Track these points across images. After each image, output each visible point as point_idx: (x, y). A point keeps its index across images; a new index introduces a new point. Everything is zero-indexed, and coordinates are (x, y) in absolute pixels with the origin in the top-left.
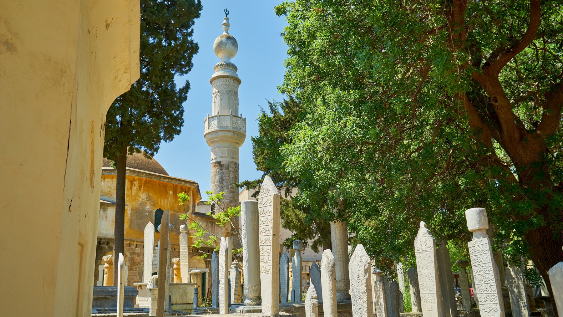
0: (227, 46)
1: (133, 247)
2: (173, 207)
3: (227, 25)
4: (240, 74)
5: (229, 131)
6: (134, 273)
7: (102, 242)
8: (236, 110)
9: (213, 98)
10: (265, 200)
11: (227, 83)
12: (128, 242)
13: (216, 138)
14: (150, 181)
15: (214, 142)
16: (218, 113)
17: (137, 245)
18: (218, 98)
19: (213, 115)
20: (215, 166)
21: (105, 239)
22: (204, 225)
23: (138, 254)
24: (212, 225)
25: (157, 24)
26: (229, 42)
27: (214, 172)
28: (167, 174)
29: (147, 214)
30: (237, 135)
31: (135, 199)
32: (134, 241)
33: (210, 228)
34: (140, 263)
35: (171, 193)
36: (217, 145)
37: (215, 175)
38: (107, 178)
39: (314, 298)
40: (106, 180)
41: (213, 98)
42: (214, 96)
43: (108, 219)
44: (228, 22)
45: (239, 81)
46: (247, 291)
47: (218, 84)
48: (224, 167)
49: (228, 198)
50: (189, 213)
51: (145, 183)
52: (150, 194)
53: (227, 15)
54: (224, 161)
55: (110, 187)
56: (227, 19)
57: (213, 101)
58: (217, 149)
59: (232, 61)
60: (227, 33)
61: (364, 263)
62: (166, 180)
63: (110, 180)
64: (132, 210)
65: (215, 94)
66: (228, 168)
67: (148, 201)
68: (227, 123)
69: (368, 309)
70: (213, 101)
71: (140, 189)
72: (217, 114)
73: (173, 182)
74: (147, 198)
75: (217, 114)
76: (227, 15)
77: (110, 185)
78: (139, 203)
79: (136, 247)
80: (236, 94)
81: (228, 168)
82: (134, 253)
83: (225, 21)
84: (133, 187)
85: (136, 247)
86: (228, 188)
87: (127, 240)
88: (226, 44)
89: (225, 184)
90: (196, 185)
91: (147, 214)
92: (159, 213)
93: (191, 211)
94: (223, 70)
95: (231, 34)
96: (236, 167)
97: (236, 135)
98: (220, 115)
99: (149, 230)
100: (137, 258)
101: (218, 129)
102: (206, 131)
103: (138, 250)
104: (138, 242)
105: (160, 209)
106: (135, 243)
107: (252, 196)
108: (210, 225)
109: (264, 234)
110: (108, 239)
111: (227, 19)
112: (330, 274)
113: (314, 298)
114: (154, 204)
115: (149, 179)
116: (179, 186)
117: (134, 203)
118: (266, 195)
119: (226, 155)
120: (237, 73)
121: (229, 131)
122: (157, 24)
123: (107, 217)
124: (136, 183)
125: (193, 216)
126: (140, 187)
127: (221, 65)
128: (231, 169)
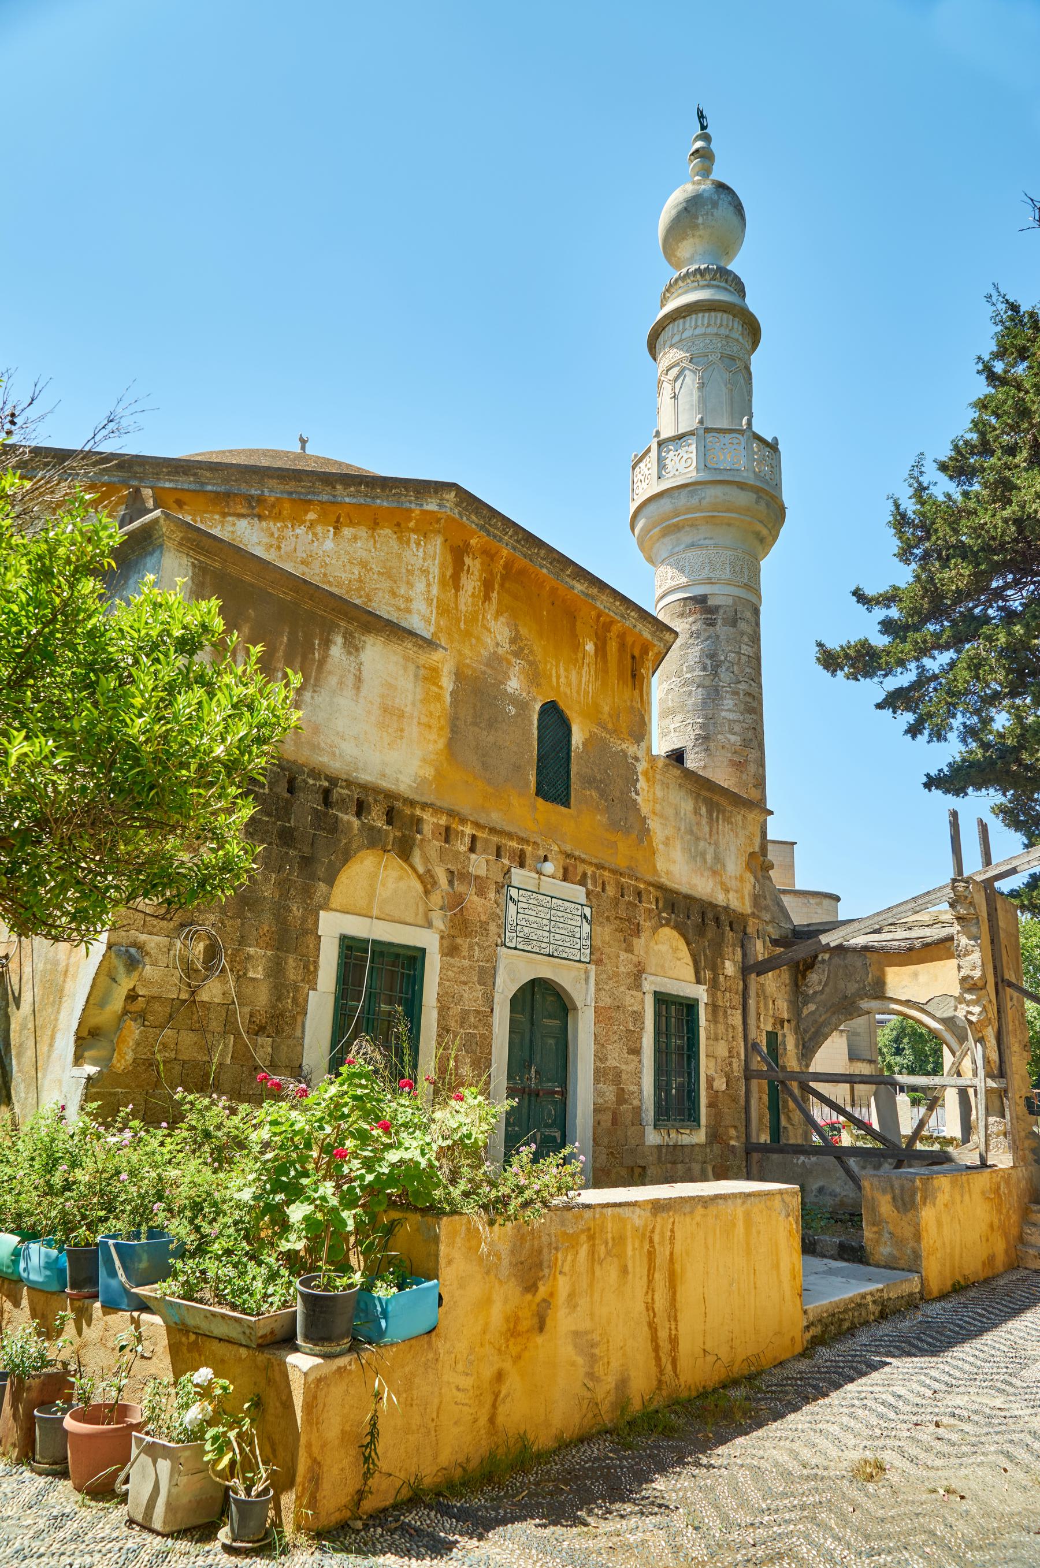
0: (717, 213)
2: (596, 707)
3: (705, 156)
5: (741, 486)
6: (462, 970)
7: (334, 797)
11: (723, 331)
12: (443, 821)
13: (689, 511)
14: (522, 572)
15: (677, 528)
18: (691, 380)
21: (349, 784)
22: (687, 806)
24: (710, 812)
25: (166, 707)
30: (768, 505)
31: (468, 634)
32: (463, 821)
33: (704, 821)
35: (590, 647)
36: (686, 538)
38: (351, 524)
40: (347, 532)
43: (364, 691)
47: (688, 333)
48: (720, 618)
49: (737, 728)
51: (504, 578)
52: (524, 631)
53: (703, 128)
54: (721, 595)
55: (364, 564)
56: (707, 138)
58: (690, 554)
62: (579, 587)
63: (363, 532)
64: (459, 676)
66: (734, 623)
67: (516, 654)
71: (487, 598)
73: (603, 602)
77: (362, 554)
78: (485, 653)
79: (472, 849)
81: (734, 623)
82: (464, 876)
83: (699, 144)
84: (463, 576)
85: (472, 849)
86: (735, 693)
88: (715, 205)
89: (725, 676)
97: (762, 506)
98: (707, 430)
100: (477, 905)
101: (704, 476)
104: (477, 825)
106: (468, 830)
107: (879, 706)
108: (704, 811)
110: (364, 787)
114: (535, 677)
115: (522, 562)
116: (615, 629)
117: (467, 651)
119: (727, 574)
121: (741, 486)
122: (166, 707)
123: (359, 679)
126: (487, 586)
127: (698, 271)
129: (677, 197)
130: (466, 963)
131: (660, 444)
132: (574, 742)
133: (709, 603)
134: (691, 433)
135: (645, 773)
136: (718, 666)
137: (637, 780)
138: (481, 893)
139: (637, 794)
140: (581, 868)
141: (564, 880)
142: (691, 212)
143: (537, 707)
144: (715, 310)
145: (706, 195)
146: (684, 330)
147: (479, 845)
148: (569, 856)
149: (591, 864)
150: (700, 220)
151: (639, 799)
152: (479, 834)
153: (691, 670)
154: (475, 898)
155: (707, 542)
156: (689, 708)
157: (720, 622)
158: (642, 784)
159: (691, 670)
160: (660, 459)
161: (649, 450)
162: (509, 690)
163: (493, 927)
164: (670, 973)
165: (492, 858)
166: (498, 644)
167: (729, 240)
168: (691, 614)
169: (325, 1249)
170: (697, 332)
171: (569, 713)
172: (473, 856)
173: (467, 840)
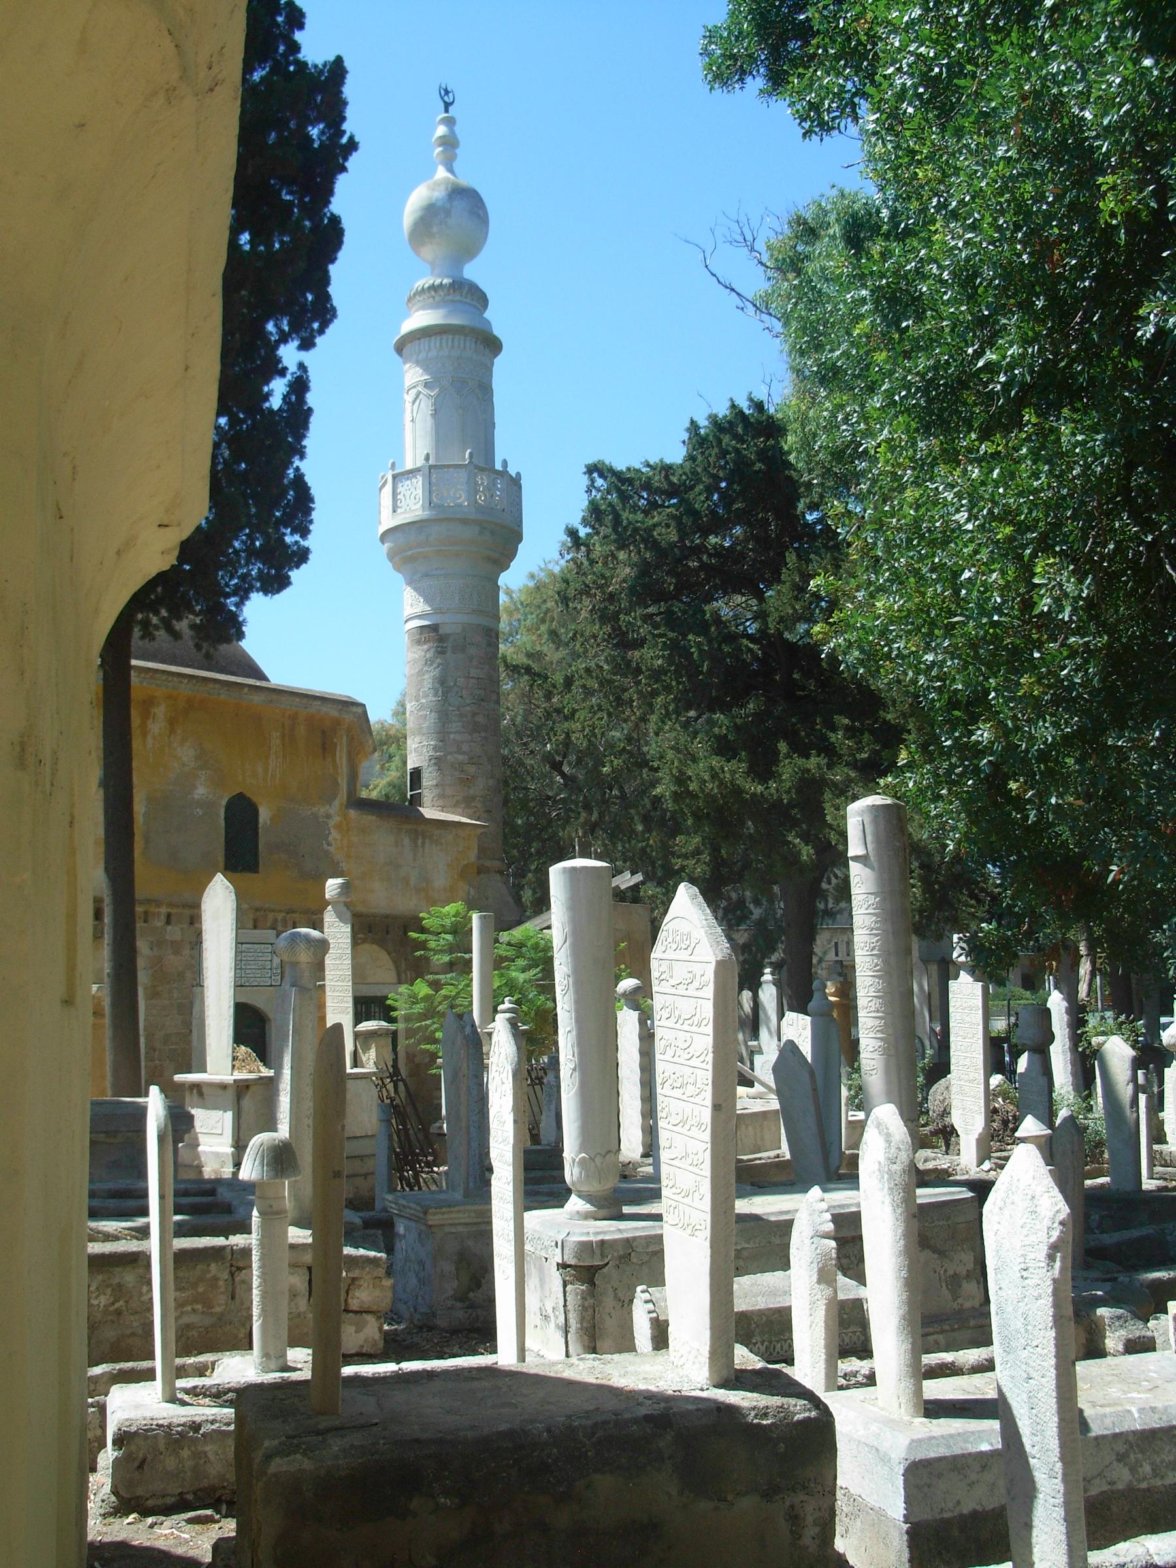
1: (159, 923)
3: (450, 143)
4: (498, 319)
5: (464, 522)
8: (486, 446)
9: (408, 406)
10: (680, 972)
16: (427, 458)
17: (169, 916)
19: (409, 466)
20: (419, 642)
23: (176, 947)
24: (415, 841)
26: (460, 205)
27: (415, 661)
28: (263, 677)
29: (200, 812)
32: (158, 903)
34: (181, 975)
37: (421, 673)
39: (826, 1236)
41: (408, 406)
42: (409, 398)
44: (452, 131)
45: (493, 345)
46: (576, 1170)
50: (337, 803)
53: (447, 106)
57: (408, 417)
59: (472, 271)
60: (451, 170)
61: (1047, 1222)
62: (257, 698)
65: (413, 392)
68: (458, 496)
69: (1059, 1387)
70: (408, 417)
71: (172, 731)
72: (420, 462)
74: (197, 758)
75: (420, 462)
76: (447, 106)
79: (168, 922)
80: (486, 390)
83: (441, 130)
85: (168, 922)
87: (141, 903)
88: (448, 213)
90: (360, 710)
91: (200, 812)
92: (241, 817)
93: (343, 796)
94: (435, 306)
95: (465, 181)
96: (489, 645)
99: (219, 902)
102: (388, 521)
103: (174, 932)
104: (170, 905)
105: (241, 796)
106: (164, 910)
109: (677, 1093)
111: (450, 122)
112: (899, 1197)
113: (826, 1236)
118: (683, 955)
120: (487, 315)
124: (160, 711)
125: (352, 813)
126: (172, 723)
127: (433, 288)
128: (472, 651)
129: (418, 197)
130: (166, 1002)
131: (394, 477)
132: (261, 820)
133: (441, 632)
134: (418, 470)
135: (338, 827)
136: (447, 692)
137: (330, 833)
138: (177, 952)
139: (329, 844)
140: (271, 916)
141: (255, 927)
142: (430, 221)
143: (224, 802)
144: (445, 332)
145: (440, 204)
146: (420, 352)
147: (173, 919)
148: (257, 910)
149: (281, 911)
150: (435, 230)
151: (332, 849)
152: (174, 911)
153: (426, 696)
154: (172, 957)
155: (438, 572)
156: (425, 731)
157: (449, 650)
158: (334, 835)
159: (426, 696)
160: (395, 494)
161: (386, 482)
162: (196, 797)
163: (188, 975)
164: (370, 980)
165: (185, 926)
166: (184, 765)
167: (469, 249)
168: (425, 642)
169: (372, 1254)
170: (430, 355)
171: (254, 799)
172: (169, 928)
173: (163, 918)
